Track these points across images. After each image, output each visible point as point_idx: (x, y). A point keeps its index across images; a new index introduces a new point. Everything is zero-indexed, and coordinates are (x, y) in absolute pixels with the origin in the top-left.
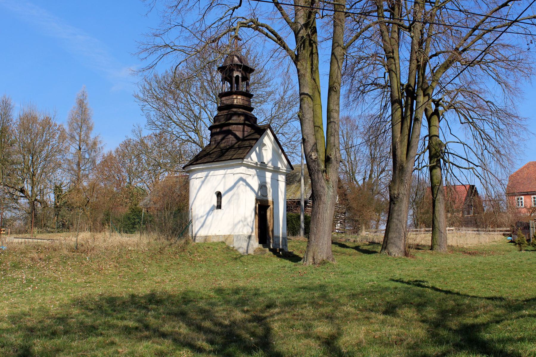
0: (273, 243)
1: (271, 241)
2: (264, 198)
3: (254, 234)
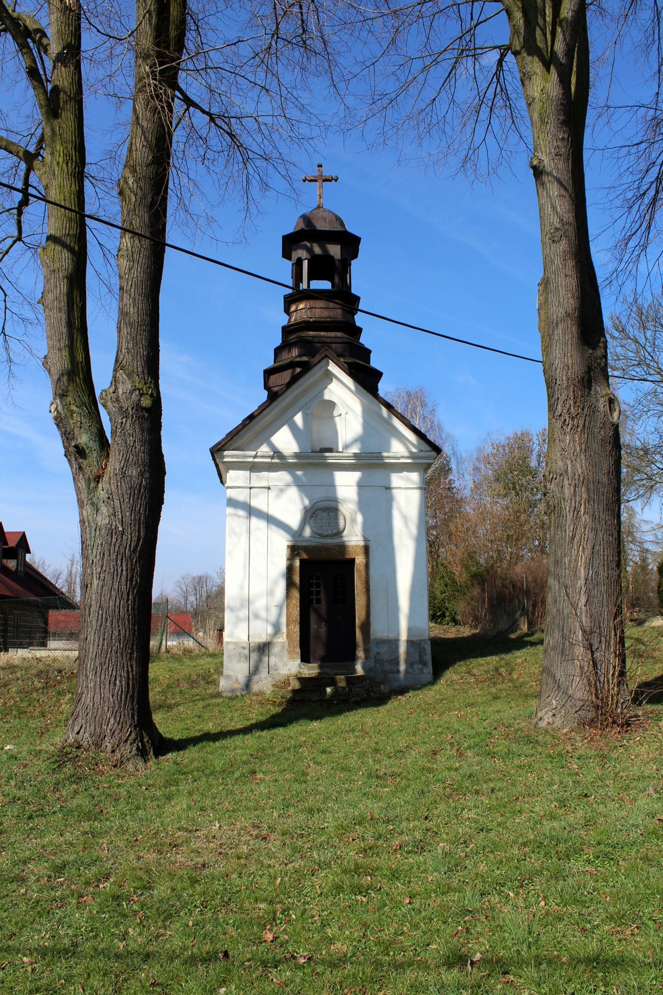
0: (367, 658)
1: (360, 653)
2: (335, 541)
3: (282, 639)
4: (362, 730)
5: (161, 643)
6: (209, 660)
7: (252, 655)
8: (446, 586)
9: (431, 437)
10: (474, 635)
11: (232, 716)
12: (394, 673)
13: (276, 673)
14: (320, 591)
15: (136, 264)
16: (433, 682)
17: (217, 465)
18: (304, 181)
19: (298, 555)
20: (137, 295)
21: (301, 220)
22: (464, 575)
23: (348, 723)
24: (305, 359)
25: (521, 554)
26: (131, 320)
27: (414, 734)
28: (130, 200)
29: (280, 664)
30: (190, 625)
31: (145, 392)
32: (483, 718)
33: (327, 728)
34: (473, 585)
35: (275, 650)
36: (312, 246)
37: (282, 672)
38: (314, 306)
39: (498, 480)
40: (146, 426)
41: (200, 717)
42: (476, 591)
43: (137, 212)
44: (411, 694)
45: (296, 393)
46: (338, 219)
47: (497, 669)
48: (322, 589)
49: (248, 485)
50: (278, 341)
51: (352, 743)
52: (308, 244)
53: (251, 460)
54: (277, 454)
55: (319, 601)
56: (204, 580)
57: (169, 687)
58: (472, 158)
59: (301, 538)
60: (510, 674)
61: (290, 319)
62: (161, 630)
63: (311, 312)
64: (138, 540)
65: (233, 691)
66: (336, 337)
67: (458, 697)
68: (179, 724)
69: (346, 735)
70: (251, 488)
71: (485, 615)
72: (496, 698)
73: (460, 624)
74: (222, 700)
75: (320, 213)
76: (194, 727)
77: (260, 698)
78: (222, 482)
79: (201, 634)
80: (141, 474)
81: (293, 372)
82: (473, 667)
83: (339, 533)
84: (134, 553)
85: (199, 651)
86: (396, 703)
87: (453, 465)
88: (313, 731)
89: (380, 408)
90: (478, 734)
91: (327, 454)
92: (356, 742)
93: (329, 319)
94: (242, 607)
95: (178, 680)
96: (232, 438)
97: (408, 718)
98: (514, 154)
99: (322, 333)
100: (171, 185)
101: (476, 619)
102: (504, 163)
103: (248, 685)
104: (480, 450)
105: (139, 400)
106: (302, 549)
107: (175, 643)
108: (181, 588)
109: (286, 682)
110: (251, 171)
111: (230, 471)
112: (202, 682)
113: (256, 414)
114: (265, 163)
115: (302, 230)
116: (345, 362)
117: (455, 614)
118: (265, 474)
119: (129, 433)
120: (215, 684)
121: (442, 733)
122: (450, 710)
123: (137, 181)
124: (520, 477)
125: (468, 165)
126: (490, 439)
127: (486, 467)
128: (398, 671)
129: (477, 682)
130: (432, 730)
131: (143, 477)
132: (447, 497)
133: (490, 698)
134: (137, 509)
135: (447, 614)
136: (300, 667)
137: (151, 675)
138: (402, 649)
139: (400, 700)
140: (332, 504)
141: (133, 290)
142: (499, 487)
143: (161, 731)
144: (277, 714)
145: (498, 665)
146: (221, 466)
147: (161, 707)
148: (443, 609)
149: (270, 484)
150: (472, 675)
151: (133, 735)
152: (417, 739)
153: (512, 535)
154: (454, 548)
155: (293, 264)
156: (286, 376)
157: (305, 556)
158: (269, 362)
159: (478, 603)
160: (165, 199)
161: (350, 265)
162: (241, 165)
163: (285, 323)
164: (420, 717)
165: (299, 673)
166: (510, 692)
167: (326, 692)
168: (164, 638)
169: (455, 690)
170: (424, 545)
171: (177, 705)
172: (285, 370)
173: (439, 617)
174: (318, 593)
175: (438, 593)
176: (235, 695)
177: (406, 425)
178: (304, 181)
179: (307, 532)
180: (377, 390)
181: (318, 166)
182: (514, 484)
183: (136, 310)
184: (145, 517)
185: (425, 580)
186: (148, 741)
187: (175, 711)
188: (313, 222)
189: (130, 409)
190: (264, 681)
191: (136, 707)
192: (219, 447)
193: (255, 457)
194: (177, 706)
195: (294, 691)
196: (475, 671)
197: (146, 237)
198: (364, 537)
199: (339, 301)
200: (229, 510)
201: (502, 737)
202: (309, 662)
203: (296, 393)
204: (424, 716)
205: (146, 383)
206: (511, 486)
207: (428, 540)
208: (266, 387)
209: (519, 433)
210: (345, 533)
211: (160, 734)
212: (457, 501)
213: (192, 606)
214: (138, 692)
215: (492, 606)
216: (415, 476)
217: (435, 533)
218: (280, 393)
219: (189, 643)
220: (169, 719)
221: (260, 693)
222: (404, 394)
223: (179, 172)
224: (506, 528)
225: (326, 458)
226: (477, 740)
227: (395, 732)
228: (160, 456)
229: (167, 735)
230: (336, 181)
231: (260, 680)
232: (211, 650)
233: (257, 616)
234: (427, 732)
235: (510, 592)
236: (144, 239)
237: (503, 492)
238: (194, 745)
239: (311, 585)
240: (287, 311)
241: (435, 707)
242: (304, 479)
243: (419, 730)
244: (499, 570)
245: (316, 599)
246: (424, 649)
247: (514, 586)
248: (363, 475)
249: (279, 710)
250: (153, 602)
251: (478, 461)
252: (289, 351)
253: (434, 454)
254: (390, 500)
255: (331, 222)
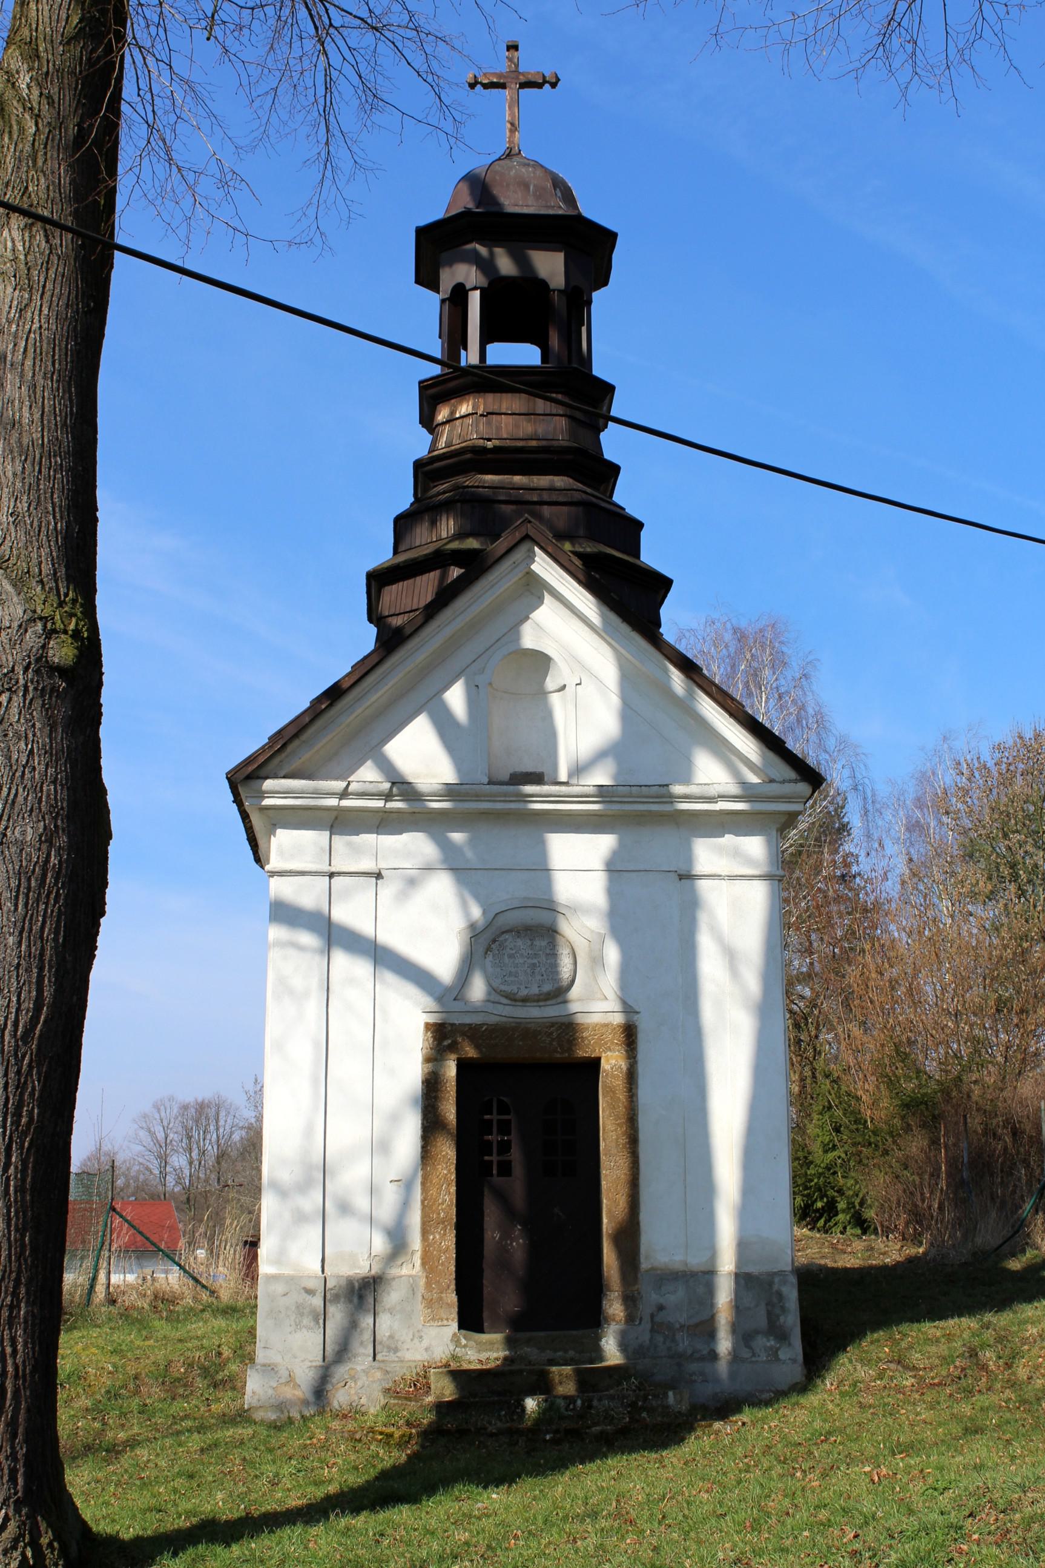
0: (630, 1319)
1: (614, 1308)
3: (411, 1268)
4: (617, 1515)
5: (94, 1279)
6: (220, 1323)
7: (332, 1309)
8: (837, 1130)
9: (793, 745)
10: (911, 1261)
11: (277, 1475)
12: (702, 1359)
13: (392, 1357)
14: (509, 1142)
15: (37, 297)
16: (804, 1387)
17: (245, 816)
18: (472, 86)
19: (453, 1048)
20: (39, 379)
21: (465, 188)
22: (885, 1103)
23: (580, 1494)
24: (473, 543)
25: (1032, 1049)
26: (25, 441)
27: (755, 1526)
28: (22, 130)
29: (404, 1335)
30: (173, 1228)
31: (59, 625)
32: (940, 1485)
33: (527, 1508)
34: (908, 1128)
35: (392, 1296)
36: (492, 254)
37: (409, 1356)
38: (496, 409)
39: (971, 856)
40: (61, 712)
41: (191, 1477)
42: (916, 1145)
43: (40, 163)
44: (746, 1415)
45: (448, 631)
46: (558, 183)
47: (973, 1353)
48: (514, 1137)
49: (326, 868)
50: (404, 500)
51: (591, 1549)
52: (483, 251)
53: (333, 802)
54: (401, 786)
55: (505, 1169)
56: (212, 1113)
57: (113, 1394)
58: (904, 23)
59: (458, 1006)
60: (1009, 1366)
61: (434, 442)
62: (93, 1242)
63: (489, 423)
64: (38, 1009)
65: (280, 1406)
66: (552, 489)
67: (872, 1427)
68: (135, 1496)
69: (577, 1526)
70: (331, 875)
71: (941, 1208)
72: (973, 1430)
73: (875, 1232)
74: (250, 1431)
75: (514, 169)
76: (175, 1505)
77: (351, 1425)
78: (258, 860)
79: (201, 1253)
80: (47, 838)
81: (443, 577)
82: (911, 1347)
83: (559, 993)
84: (25, 1043)
85: (195, 1299)
86: (707, 1441)
87: (853, 817)
88: (488, 1516)
89: (666, 671)
90: (927, 1529)
91: (529, 789)
92: (601, 1547)
93: (534, 443)
94: (303, 1187)
95: (136, 1377)
96: (284, 746)
97: (739, 1482)
98: (1014, 11)
99: (517, 479)
100: (129, 91)
101: (917, 1217)
102: (987, 33)
103: (320, 1392)
104: (924, 778)
105: (44, 647)
106: (463, 1034)
107: (131, 1278)
108: (152, 1134)
109: (420, 1383)
110: (336, 59)
111: (279, 831)
112: (200, 1383)
113: (345, 685)
114: (370, 37)
115: (466, 214)
116: (575, 553)
117: (862, 1204)
118: (368, 839)
119: (16, 732)
120: (234, 1388)
121: (828, 1524)
122: (850, 1460)
123: (41, 80)
124: (1029, 848)
125: (895, 42)
126: (950, 749)
127: (940, 822)
128: (714, 1356)
129: (922, 1386)
130: (803, 1515)
131: (51, 845)
132: (838, 899)
133: (957, 1429)
134: (36, 928)
135: (842, 1205)
136: (457, 1343)
137: (65, 1364)
138: (724, 1295)
139: (719, 1431)
140: (542, 917)
141: (29, 363)
142: (975, 875)
143: (87, 1514)
144: (394, 1467)
145: (976, 1342)
146: (256, 819)
147: (88, 1448)
148: (831, 1193)
149: (382, 865)
150: (907, 1368)
151: (12, 1526)
152: (762, 1539)
153: (1011, 998)
154: (857, 1032)
155: (443, 301)
156: (425, 587)
157: (471, 1052)
158: (382, 554)
159: (920, 1175)
160: (111, 129)
161: (589, 302)
162: (310, 44)
163: (422, 452)
164: (771, 1479)
165: (454, 1357)
166: (1008, 1415)
167: (523, 1409)
168: (103, 1264)
169: (861, 1406)
170: (780, 1023)
171: (132, 1443)
172: (422, 573)
173: (821, 1212)
174: (504, 1147)
175: (816, 1148)
176: (284, 1416)
177: (731, 715)
178: (472, 86)
179: (478, 990)
180: (658, 624)
181: (509, 48)
182: (1013, 866)
183: (37, 416)
184: (56, 948)
185: (781, 1115)
186: (50, 1545)
187: (126, 1460)
188: (495, 191)
189: (19, 670)
190: (363, 1380)
191: (22, 1452)
192: (250, 769)
193: (344, 794)
194: (132, 1447)
195: (441, 1408)
196: (915, 1357)
197: (64, 228)
198: (624, 1002)
199: (560, 397)
200: (276, 932)
201: (991, 1539)
202: (480, 1330)
203: (448, 631)
204: (781, 1476)
205: (61, 604)
206: (1006, 871)
207: (791, 1011)
208: (374, 616)
209: (1029, 734)
210: (575, 992)
211: (84, 1523)
212: (866, 910)
213: (179, 1180)
214: (28, 1410)
215: (957, 1184)
216: (755, 846)
217: (807, 992)
218: (408, 631)
219: (170, 1278)
220: (108, 1482)
221: (353, 1413)
222: (728, 636)
223: (150, 60)
224: (992, 979)
225: (525, 798)
226: (923, 1544)
227: (705, 1519)
228: (99, 792)
229: (102, 1527)
230: (554, 85)
231: (353, 1378)
232: (225, 1296)
233: (345, 1208)
234: (789, 1520)
235: (1006, 1149)
236: (58, 232)
237: (985, 887)
238: (175, 1554)
239: (487, 1127)
240: (427, 420)
241: (810, 1453)
242: (469, 854)
243: (768, 1515)
244: (977, 1091)
245: (499, 1163)
246: (780, 1295)
247: (1015, 1133)
248: (621, 843)
249: (400, 1457)
250: (75, 1167)
251: (920, 808)
252: (433, 523)
253: (804, 788)
254: (690, 906)
255: (539, 194)
